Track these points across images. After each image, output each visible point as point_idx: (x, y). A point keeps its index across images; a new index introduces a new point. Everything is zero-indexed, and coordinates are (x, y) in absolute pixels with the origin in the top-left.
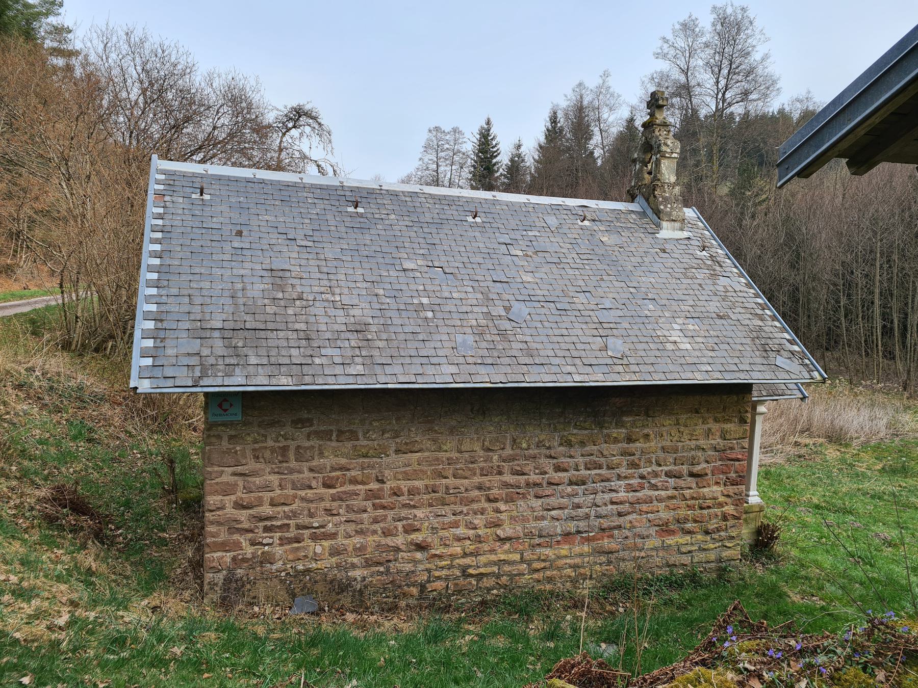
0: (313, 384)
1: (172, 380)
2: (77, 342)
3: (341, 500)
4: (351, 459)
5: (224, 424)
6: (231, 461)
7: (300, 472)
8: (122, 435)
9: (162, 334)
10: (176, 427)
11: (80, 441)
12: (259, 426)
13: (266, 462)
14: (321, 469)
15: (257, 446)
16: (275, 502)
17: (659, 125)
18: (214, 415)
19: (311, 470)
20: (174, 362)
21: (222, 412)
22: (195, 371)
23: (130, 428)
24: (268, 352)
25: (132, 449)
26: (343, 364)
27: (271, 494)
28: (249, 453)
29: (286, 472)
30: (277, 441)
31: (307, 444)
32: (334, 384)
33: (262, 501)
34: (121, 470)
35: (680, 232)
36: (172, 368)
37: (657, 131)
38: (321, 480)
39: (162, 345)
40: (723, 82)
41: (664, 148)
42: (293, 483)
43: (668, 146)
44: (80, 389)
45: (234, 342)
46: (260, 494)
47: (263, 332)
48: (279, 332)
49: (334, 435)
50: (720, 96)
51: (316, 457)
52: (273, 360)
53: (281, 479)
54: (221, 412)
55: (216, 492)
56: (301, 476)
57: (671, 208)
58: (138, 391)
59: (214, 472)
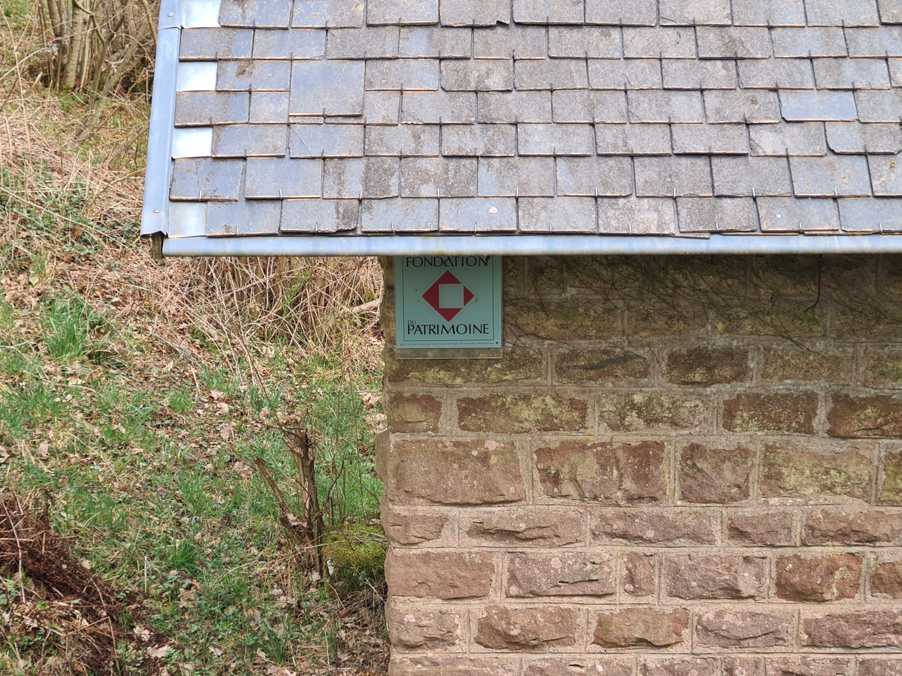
0: (751, 232)
1: (272, 209)
2: (80, 64)
3: (845, 645)
4: (879, 502)
5: (445, 361)
6: (471, 488)
7: (696, 537)
8: (182, 344)
9: (241, 46)
10: (326, 323)
11: (71, 359)
12: (561, 371)
13: (582, 497)
14: (772, 532)
15: (552, 439)
16: (615, 633)
18: (412, 327)
19: (737, 533)
20: (281, 143)
21: (438, 319)
22: (347, 177)
23: (202, 323)
24: (591, 107)
25: (206, 389)
26: (865, 154)
27: (601, 606)
28: (527, 464)
29: (650, 534)
30: (619, 425)
31: (724, 441)
32: (833, 233)
33: (571, 628)
34: (174, 451)
36: (273, 164)
38: (770, 570)
39: (242, 84)
42: (675, 573)
44: (76, 205)
45: (475, 72)
46: (566, 604)
47: (575, 34)
48: (629, 33)
49: (822, 413)
51: (755, 490)
52: (609, 140)
53: (634, 558)
54: (430, 316)
55: (423, 588)
56: (703, 550)
58: (168, 247)
59: (416, 519)
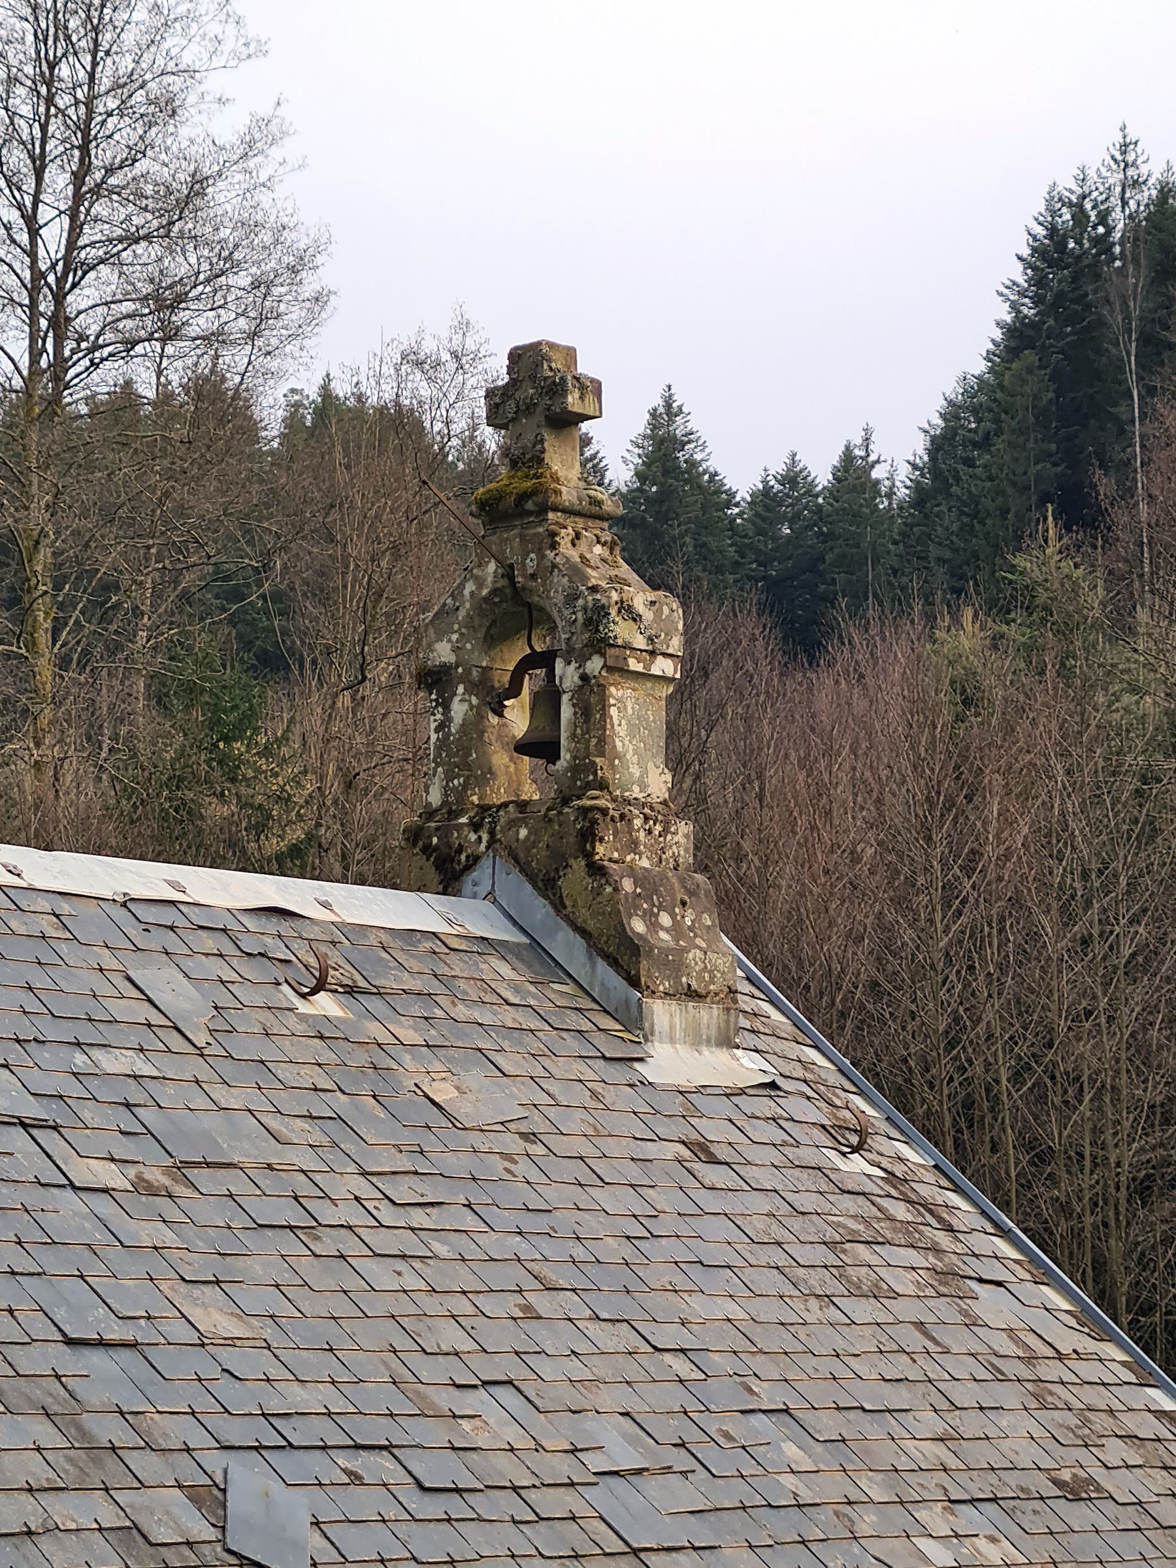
17: (569, 512)
35: (721, 1056)
37: (565, 537)
40: (54, 237)
41: (622, 630)
43: (636, 618)
50: (46, 306)
57: (677, 930)
